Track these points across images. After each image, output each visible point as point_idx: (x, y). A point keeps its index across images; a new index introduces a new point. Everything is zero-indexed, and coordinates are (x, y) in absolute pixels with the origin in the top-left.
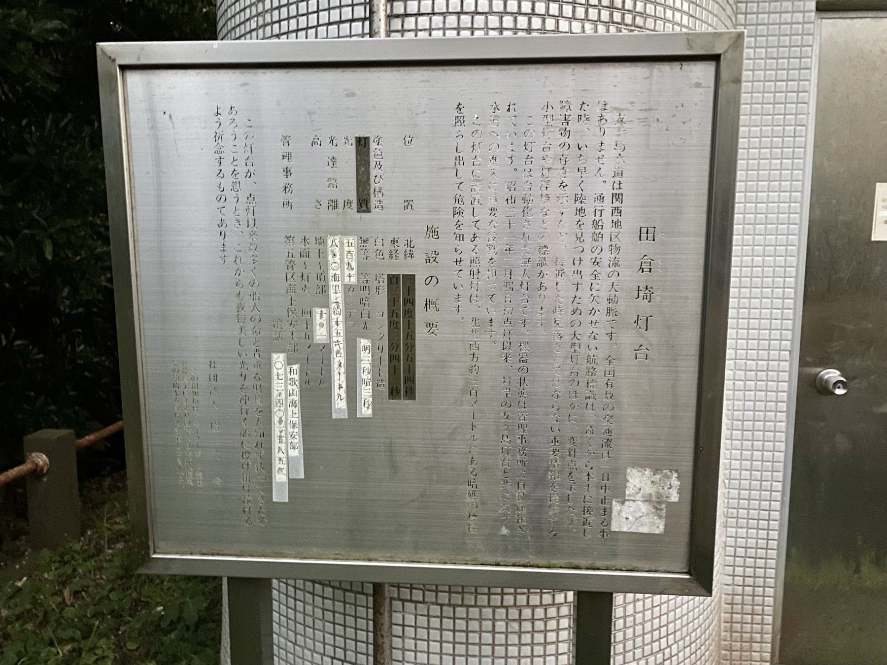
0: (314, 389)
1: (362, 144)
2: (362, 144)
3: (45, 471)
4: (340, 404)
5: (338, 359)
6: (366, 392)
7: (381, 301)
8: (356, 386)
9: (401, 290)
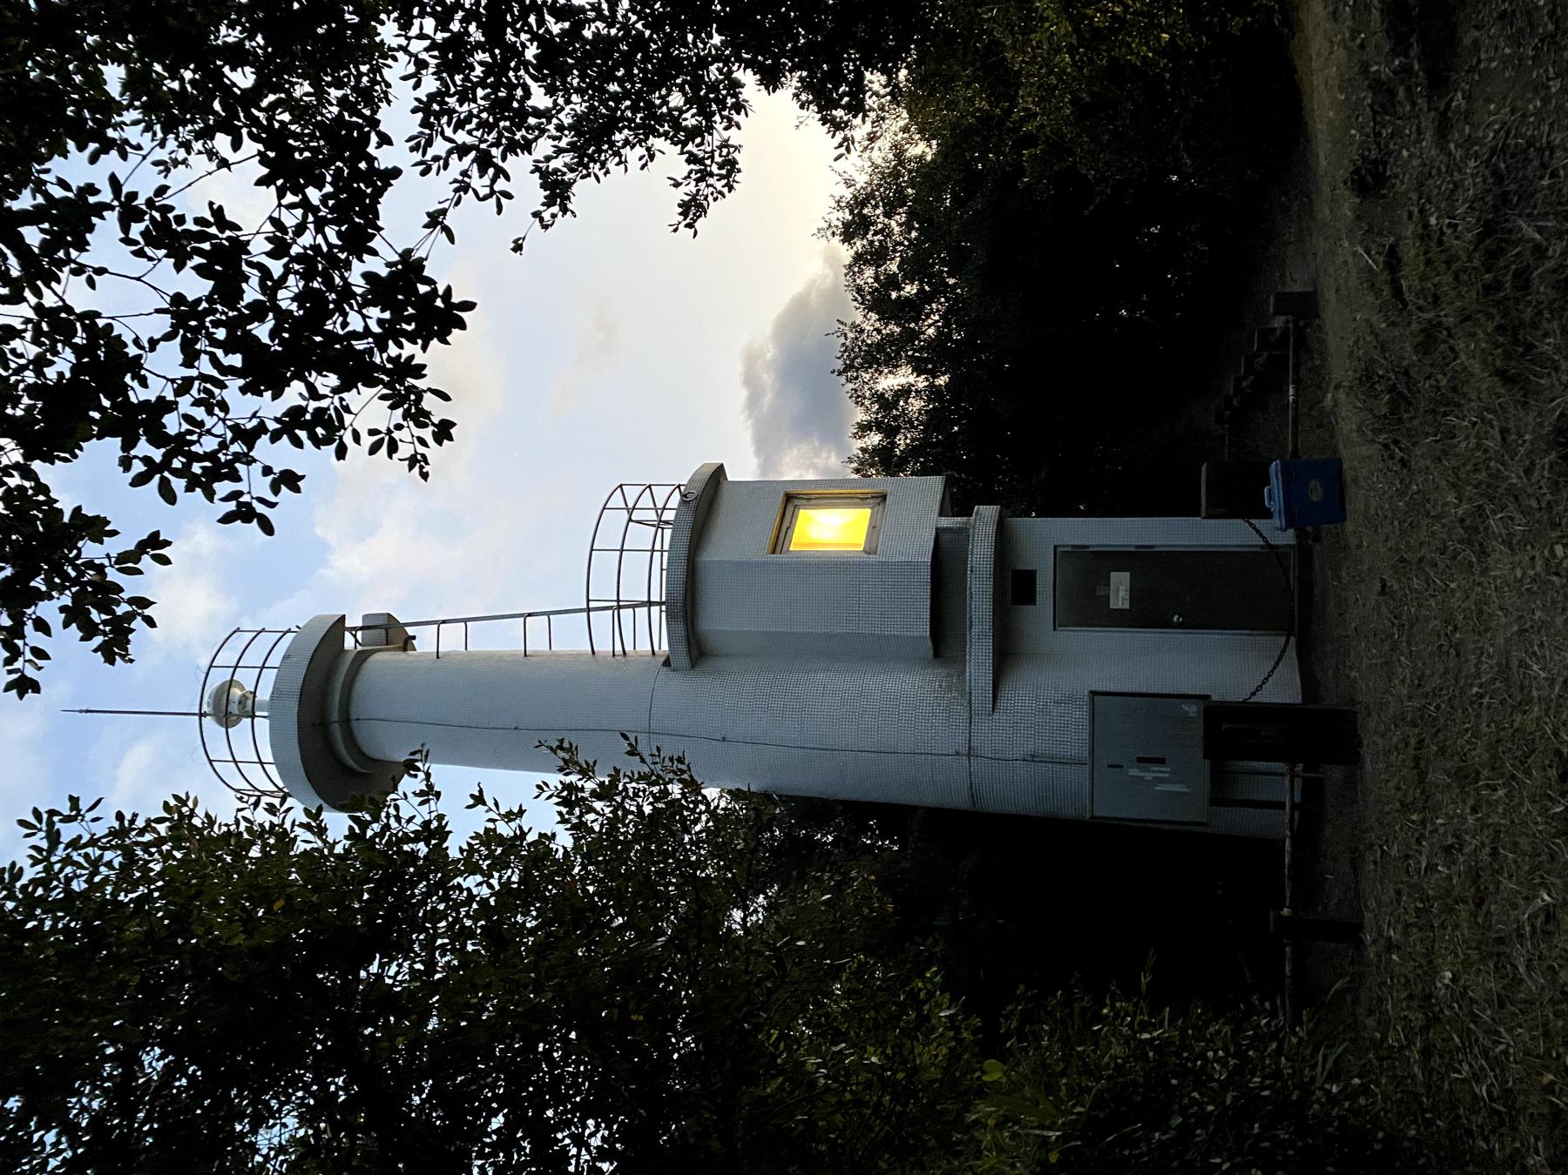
9: (1140, 760)
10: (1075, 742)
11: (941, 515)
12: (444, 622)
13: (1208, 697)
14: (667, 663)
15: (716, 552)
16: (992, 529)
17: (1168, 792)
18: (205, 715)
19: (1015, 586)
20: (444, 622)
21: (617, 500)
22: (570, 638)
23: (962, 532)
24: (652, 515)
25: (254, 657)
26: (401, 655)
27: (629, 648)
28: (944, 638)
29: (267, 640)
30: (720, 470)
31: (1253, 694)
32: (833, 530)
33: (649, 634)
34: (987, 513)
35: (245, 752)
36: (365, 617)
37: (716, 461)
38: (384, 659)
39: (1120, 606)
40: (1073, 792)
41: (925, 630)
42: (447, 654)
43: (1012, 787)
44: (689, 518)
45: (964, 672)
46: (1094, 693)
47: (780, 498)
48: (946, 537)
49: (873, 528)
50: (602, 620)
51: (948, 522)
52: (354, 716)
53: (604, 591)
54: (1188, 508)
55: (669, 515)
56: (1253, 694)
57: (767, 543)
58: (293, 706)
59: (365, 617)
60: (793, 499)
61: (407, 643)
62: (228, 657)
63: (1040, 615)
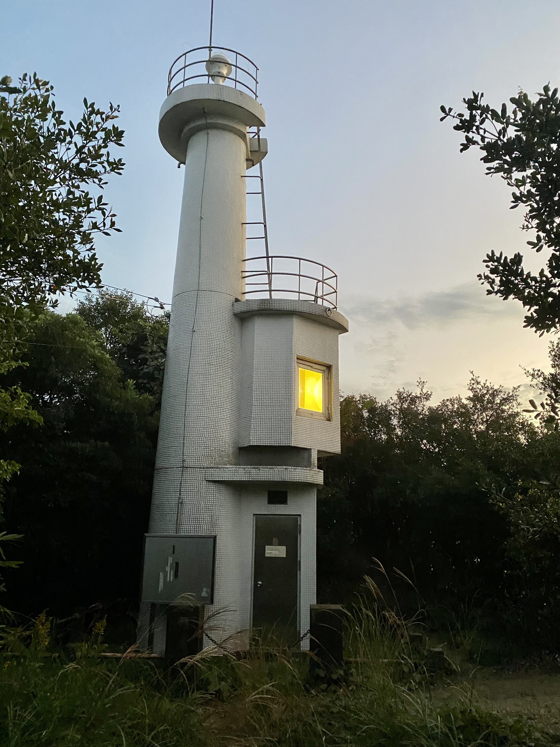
0: (165, 577)
1: (174, 546)
2: (174, 546)
3: (557, 284)
4: (168, 579)
5: (168, 573)
6: (172, 578)
7: (175, 565)
8: (170, 577)
9: (177, 564)
10: (188, 528)
11: (319, 451)
12: (262, 180)
13: (212, 602)
14: (237, 300)
15: (297, 325)
16: (309, 480)
17: (159, 578)
18: (210, 50)
19: (278, 493)
20: (262, 180)
21: (328, 274)
22: (254, 249)
23: (309, 465)
24: (320, 294)
25: (242, 76)
26: (243, 157)
27: (247, 280)
28: (250, 453)
29: (251, 83)
30: (345, 330)
31: (207, 635)
32: (311, 392)
33: (254, 292)
34: (318, 477)
35: (190, 71)
36: (266, 140)
37: (349, 330)
38: (241, 150)
39: (267, 551)
40: (163, 525)
41: (254, 442)
42: (244, 182)
43: (165, 492)
44: (318, 312)
45: (231, 464)
46: (215, 538)
47: (328, 362)
48: (306, 455)
49: (312, 414)
50: (262, 265)
51: (314, 456)
52: (209, 131)
53: (277, 265)
54: (321, 596)
55: (320, 301)
56: (207, 635)
57: (302, 354)
58: (213, 96)
59: (266, 140)
60: (328, 370)
61: (251, 162)
62: (242, 62)
63: (266, 508)
